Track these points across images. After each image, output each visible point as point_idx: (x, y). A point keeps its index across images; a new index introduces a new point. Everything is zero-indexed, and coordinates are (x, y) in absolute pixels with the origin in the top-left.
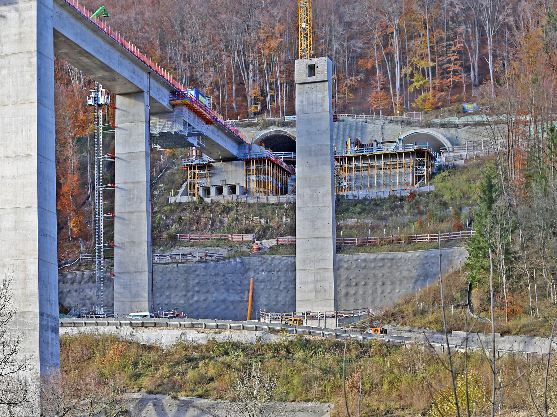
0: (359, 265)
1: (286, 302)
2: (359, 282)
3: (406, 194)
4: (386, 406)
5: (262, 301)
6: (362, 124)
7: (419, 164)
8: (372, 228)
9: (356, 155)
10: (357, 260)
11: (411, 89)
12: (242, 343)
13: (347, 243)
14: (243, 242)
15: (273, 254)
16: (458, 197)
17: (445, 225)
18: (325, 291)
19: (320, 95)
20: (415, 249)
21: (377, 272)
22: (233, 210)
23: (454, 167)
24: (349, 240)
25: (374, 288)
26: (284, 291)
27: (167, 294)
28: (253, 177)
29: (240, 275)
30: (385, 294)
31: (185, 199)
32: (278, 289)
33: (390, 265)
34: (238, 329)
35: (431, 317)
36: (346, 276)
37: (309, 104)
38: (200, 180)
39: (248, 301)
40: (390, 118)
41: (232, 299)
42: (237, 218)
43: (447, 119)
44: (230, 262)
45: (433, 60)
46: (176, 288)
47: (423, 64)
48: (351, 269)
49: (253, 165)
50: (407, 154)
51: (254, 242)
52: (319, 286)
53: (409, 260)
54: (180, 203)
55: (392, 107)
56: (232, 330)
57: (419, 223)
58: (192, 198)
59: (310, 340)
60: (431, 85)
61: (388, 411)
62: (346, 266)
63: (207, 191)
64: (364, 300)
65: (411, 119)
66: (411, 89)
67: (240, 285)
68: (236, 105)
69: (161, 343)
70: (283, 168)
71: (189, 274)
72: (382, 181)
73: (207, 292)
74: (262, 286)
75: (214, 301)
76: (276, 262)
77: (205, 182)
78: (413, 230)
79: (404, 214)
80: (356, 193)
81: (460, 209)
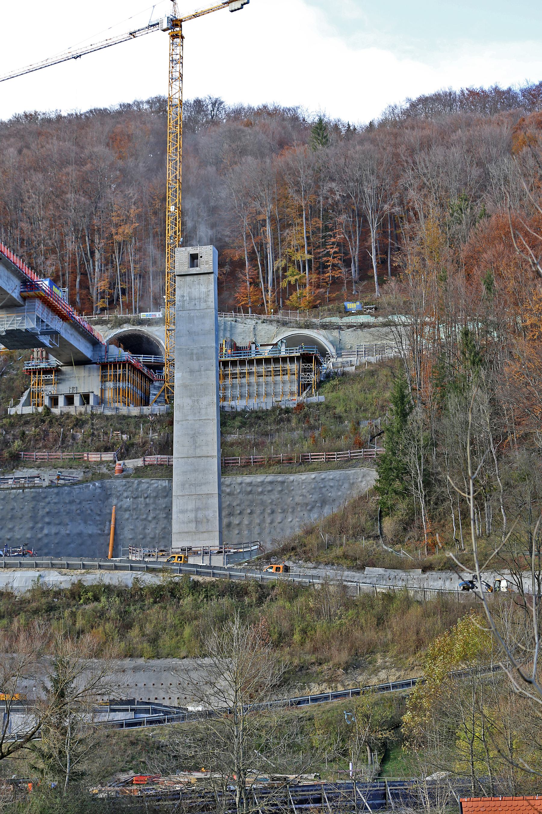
0: (244, 490)
1: (155, 535)
2: (244, 510)
3: (292, 405)
4: (300, 660)
5: (127, 534)
6: (231, 324)
7: (305, 371)
8: (256, 445)
9: (232, 359)
10: (241, 483)
11: (284, 284)
12: (115, 587)
13: (228, 463)
14: (101, 462)
15: (139, 477)
16: (354, 410)
17: (342, 442)
18: (208, 521)
19: (203, 289)
20: (310, 470)
21: (265, 498)
22: (87, 423)
23: (344, 374)
24: (230, 460)
25: (261, 517)
26: (154, 522)
27: (10, 526)
28: (110, 384)
29: (99, 502)
30: (275, 524)
31: (28, 410)
32: (145, 519)
33: (280, 489)
34: (109, 568)
35: (339, 551)
36: (228, 503)
37: (191, 299)
38: (44, 387)
39: (109, 534)
40: (263, 317)
41: (90, 532)
42: (93, 433)
43: (328, 320)
44: (88, 487)
45: (309, 252)
46: (21, 518)
47: (298, 257)
48: (233, 494)
49: (111, 369)
50: (292, 359)
51: (115, 462)
52: (200, 515)
53: (302, 483)
54: (22, 415)
55: (263, 304)
56: (102, 571)
57: (312, 439)
58: (36, 409)
59: (198, 581)
60: (307, 281)
61: (303, 667)
62: (228, 490)
63: (54, 401)
64: (250, 530)
65: (287, 319)
66: (284, 284)
67: (99, 515)
68: (80, 299)
69: (12, 588)
70: (144, 374)
71: (38, 501)
72: (263, 390)
73: (59, 524)
74: (127, 516)
75: (68, 535)
76: (144, 486)
77: (51, 389)
78: (305, 448)
79: (292, 430)
80: (233, 403)
81: (358, 423)
